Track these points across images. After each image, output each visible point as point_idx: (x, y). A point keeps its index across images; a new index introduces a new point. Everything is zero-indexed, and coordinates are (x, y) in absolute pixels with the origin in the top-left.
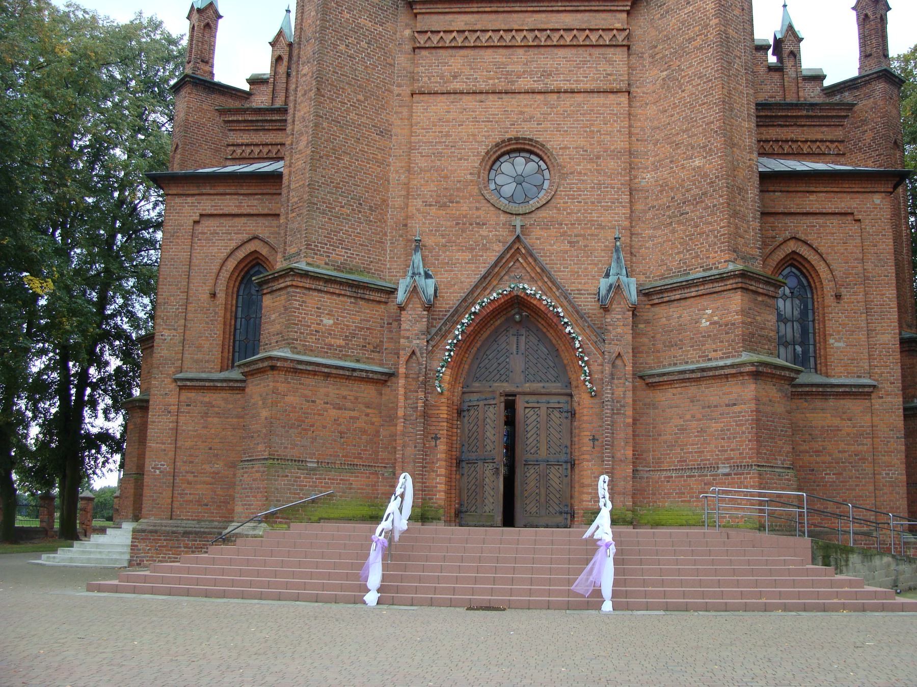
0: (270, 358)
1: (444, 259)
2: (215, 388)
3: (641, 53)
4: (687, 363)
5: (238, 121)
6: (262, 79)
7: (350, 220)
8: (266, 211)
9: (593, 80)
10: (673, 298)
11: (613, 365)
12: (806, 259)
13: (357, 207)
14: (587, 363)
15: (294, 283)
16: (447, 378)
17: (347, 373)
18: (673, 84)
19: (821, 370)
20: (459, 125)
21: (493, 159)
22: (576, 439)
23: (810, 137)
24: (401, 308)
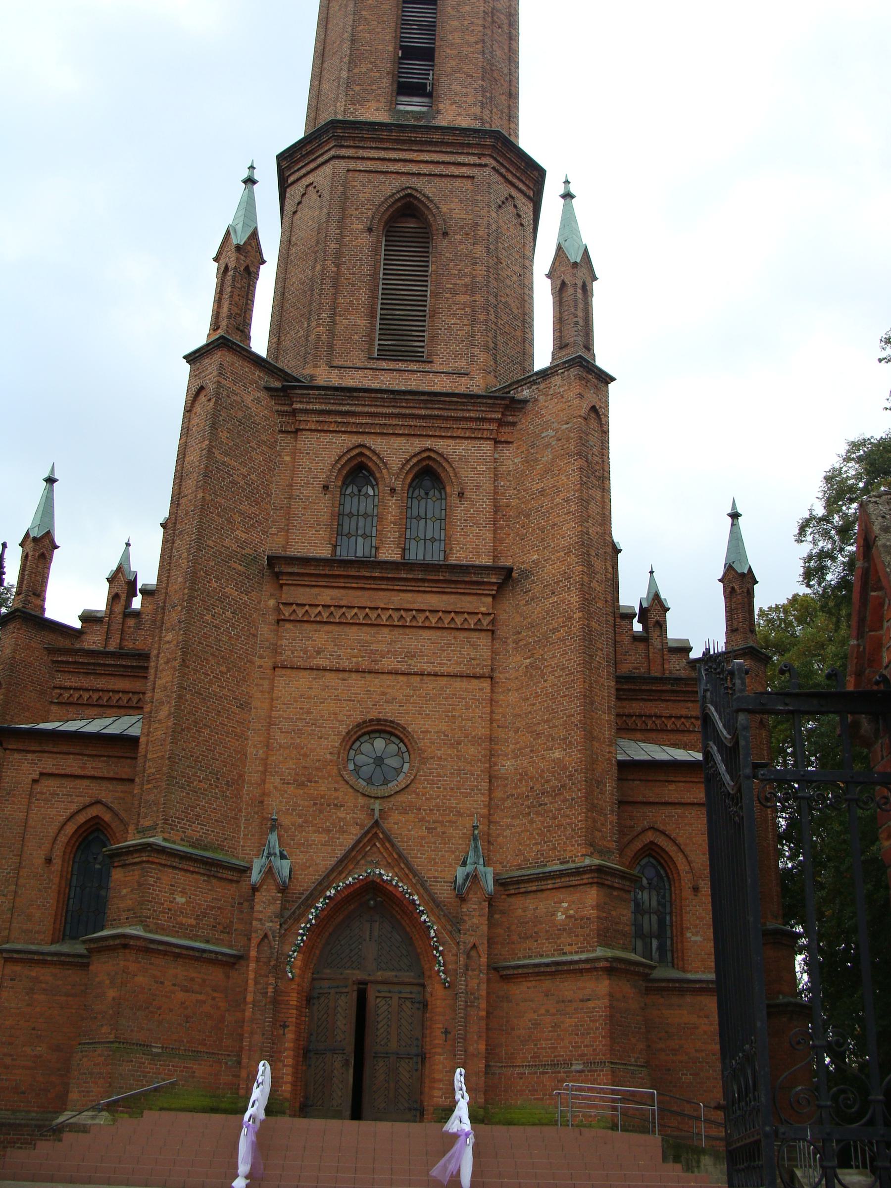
0: (124, 936)
1: (300, 840)
2: (44, 963)
3: (506, 638)
4: (542, 956)
5: (68, 662)
6: (96, 617)
7: (207, 795)
8: (111, 775)
9: (457, 663)
10: (530, 889)
11: (468, 956)
12: (664, 850)
13: (214, 781)
14: (441, 953)
15: (151, 859)
16: (299, 963)
17: (197, 954)
18: (536, 673)
19: (678, 965)
20: (321, 703)
21: (353, 739)
22: (428, 1032)
23: (675, 712)
24: (255, 889)
